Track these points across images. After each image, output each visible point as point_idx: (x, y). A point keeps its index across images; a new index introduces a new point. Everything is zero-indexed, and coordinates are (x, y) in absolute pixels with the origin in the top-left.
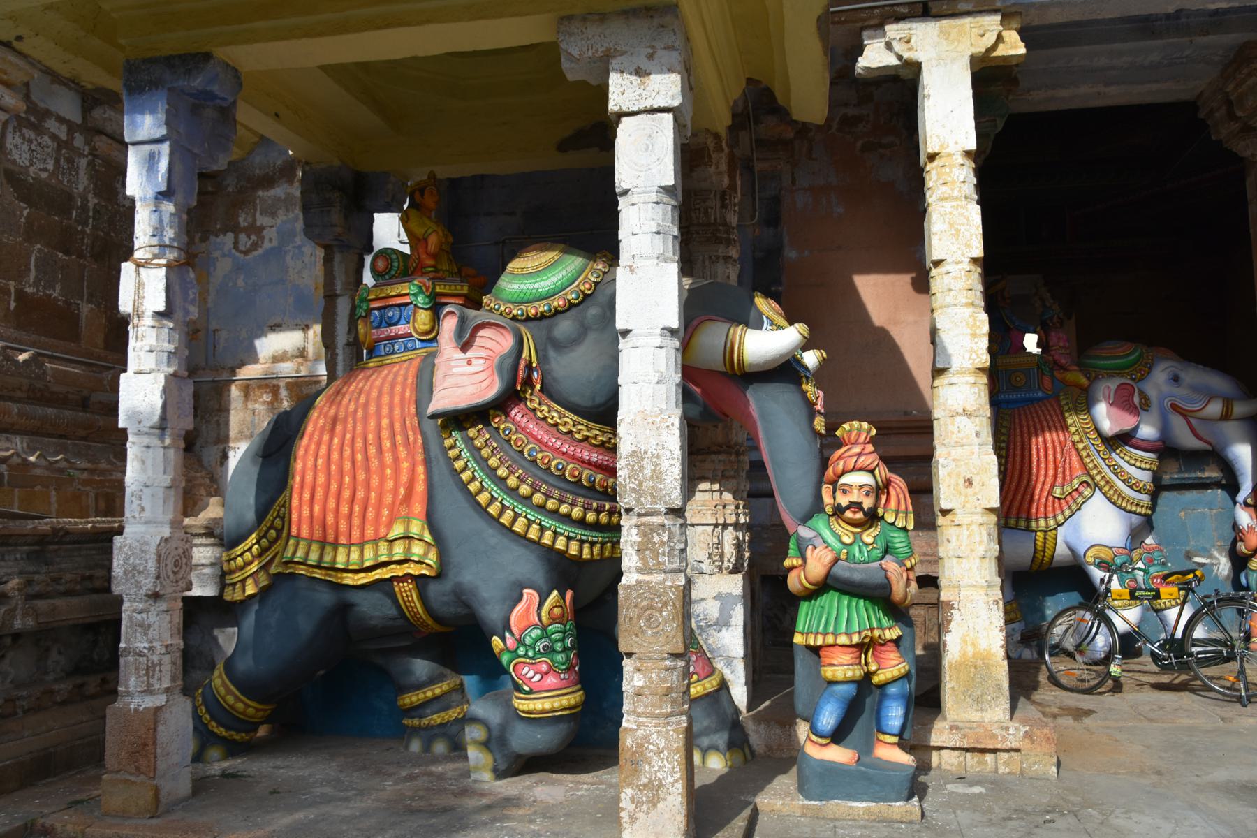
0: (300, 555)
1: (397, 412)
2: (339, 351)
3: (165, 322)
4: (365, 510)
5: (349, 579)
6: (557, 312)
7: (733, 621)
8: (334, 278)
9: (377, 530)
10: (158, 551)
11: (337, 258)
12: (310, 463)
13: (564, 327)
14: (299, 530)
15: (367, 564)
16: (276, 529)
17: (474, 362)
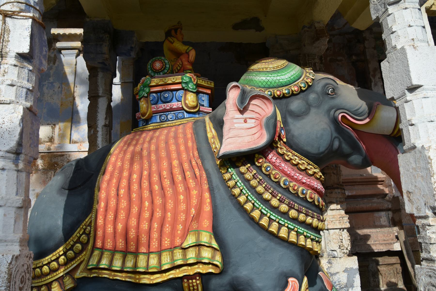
0: (104, 263)
1: (184, 156)
2: (100, 129)
3: (26, 64)
4: (162, 226)
5: (146, 280)
6: (293, 95)
7: (355, 285)
8: (97, 86)
9: (172, 241)
10: (9, 269)
11: (100, 75)
12: (113, 193)
13: (296, 105)
14: (103, 243)
15: (165, 267)
16: (81, 243)
17: (248, 120)
